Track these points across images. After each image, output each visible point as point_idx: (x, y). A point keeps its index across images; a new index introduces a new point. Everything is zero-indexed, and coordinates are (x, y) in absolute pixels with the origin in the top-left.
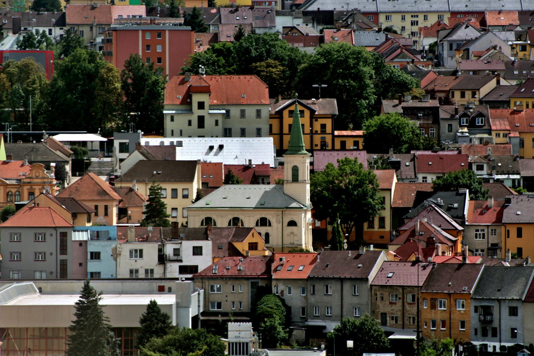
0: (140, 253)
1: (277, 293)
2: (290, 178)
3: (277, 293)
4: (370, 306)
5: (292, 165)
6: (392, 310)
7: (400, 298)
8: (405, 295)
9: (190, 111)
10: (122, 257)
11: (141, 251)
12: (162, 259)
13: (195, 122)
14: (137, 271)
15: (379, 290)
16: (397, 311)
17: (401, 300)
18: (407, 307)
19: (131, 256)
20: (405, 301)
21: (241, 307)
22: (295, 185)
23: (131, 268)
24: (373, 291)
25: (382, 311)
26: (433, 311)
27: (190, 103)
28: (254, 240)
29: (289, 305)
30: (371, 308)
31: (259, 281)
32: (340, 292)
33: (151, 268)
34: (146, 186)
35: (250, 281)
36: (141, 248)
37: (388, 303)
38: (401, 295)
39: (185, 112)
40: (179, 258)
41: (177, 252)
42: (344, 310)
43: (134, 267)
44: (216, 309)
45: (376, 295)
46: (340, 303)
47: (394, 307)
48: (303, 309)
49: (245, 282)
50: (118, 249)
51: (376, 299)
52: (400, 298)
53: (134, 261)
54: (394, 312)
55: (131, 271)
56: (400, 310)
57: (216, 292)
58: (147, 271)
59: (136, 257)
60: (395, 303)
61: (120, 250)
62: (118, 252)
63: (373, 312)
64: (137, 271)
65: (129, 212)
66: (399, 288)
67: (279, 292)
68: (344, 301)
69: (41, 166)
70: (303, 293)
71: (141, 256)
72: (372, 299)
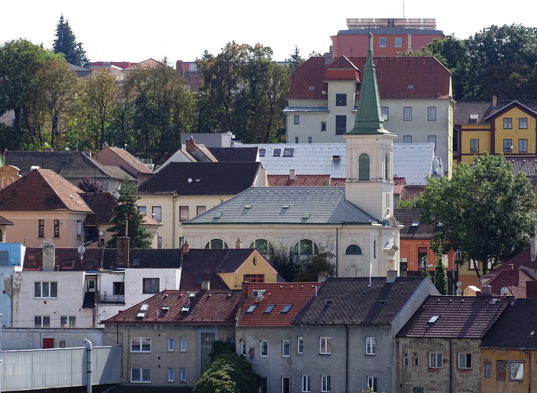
0: (53, 289)
1: (244, 353)
2: (356, 175)
3: (244, 353)
4: (394, 374)
5: (360, 152)
6: (433, 382)
7: (445, 361)
8: (455, 354)
9: (325, 109)
10: (21, 295)
11: (54, 285)
12: (91, 300)
13: (332, 125)
14: (47, 320)
15: (410, 347)
16: (440, 385)
17: (447, 365)
18: (457, 375)
19: (37, 294)
20: (454, 365)
21: (184, 378)
22: (364, 185)
23: (38, 314)
24: (401, 348)
25: (415, 384)
26: (501, 383)
27: (326, 97)
28: (256, 271)
29: (263, 375)
30: (398, 380)
31: (216, 331)
32: (345, 350)
33: (72, 314)
34: (174, 202)
35: (200, 331)
36: (54, 280)
37: (425, 369)
38: (448, 355)
39: (318, 110)
40: (121, 298)
41: (119, 288)
42: (351, 382)
43: (42, 313)
44: (141, 381)
45: (406, 355)
46: (344, 370)
47: (435, 375)
48: (287, 381)
49: (192, 333)
50: (15, 281)
51: (406, 363)
52: (445, 361)
53: (43, 302)
54: (436, 386)
55: (37, 320)
56: (445, 382)
57: (141, 351)
58: (63, 320)
59: (46, 294)
60: (437, 370)
61: (18, 283)
62: (14, 286)
63: (401, 386)
64: (47, 320)
65: (101, 233)
66: (443, 342)
67: (247, 351)
68: (350, 367)
69: (14, 169)
70: (287, 353)
71: (54, 293)
72: (398, 363)
